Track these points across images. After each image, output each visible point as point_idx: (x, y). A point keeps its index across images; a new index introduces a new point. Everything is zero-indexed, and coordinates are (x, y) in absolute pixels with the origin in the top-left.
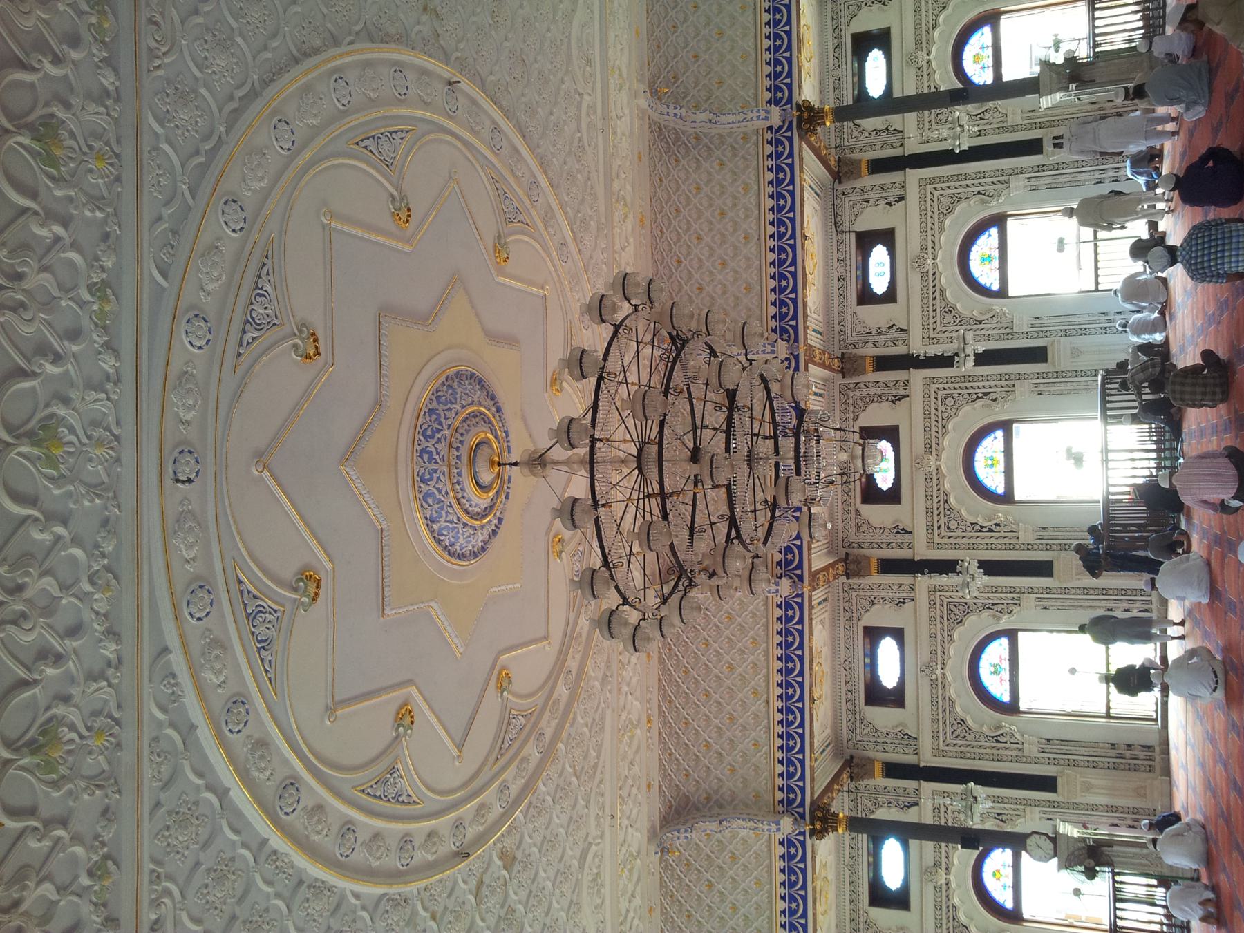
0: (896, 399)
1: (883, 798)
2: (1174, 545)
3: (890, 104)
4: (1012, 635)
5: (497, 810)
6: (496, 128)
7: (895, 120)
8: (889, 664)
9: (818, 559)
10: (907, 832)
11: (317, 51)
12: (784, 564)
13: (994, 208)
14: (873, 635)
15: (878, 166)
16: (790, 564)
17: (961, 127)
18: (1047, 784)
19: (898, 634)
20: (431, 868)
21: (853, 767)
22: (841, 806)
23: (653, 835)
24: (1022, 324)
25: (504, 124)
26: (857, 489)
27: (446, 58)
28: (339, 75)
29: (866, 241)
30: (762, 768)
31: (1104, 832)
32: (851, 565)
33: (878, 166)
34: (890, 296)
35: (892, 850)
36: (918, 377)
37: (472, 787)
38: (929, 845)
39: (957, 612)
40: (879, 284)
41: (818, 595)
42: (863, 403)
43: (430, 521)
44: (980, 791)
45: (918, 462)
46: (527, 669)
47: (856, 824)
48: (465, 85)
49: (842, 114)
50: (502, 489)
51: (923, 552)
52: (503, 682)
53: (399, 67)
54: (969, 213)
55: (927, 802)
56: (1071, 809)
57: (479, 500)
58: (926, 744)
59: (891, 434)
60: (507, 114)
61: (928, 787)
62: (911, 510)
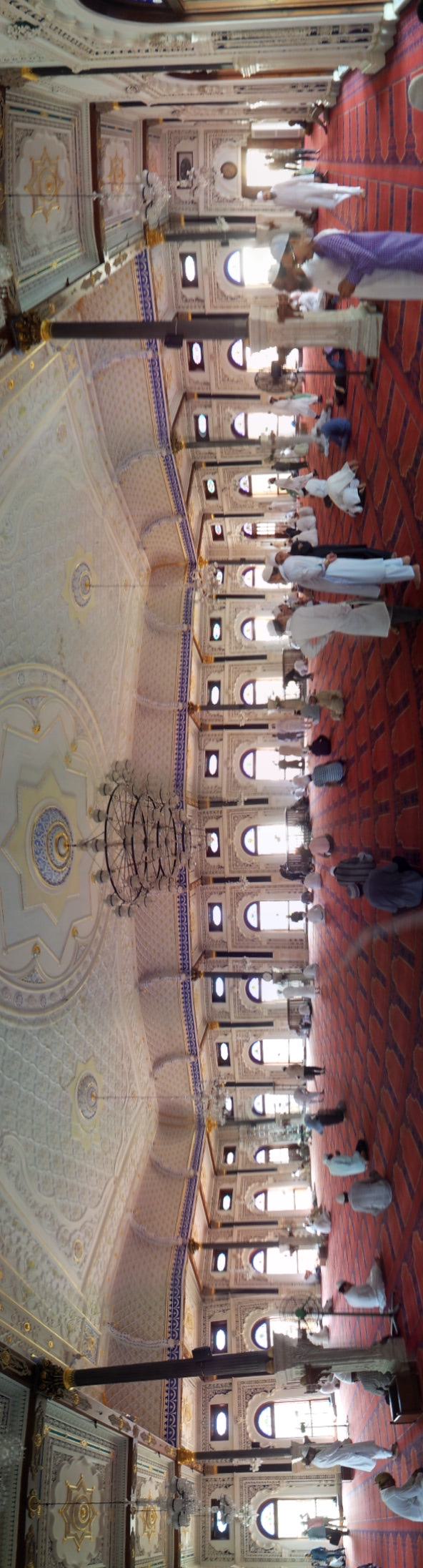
0: (218, 818)
1: (216, 965)
2: (309, 869)
3: (219, 707)
4: (258, 903)
5: (77, 982)
6: (79, 699)
7: (221, 712)
8: (217, 918)
9: (192, 878)
10: (224, 976)
11: (13, 663)
12: (179, 881)
13: (252, 746)
14: (211, 906)
15: (215, 727)
16: (182, 881)
17: (242, 717)
18: (269, 955)
19: (220, 905)
20: (53, 1006)
21: (206, 954)
22: (202, 968)
23: (136, 985)
24: (260, 789)
25: (83, 698)
26: (205, 852)
27: (64, 671)
28: (21, 673)
29: (209, 754)
30: (176, 960)
31: (287, 970)
32: (203, 880)
33: (215, 727)
34: (216, 775)
35: (219, 981)
36: (225, 809)
37: (66, 974)
38: (231, 980)
39: (239, 896)
40: (213, 771)
41: (192, 892)
42: (206, 819)
43: (41, 870)
44: (248, 959)
45: (226, 841)
46: (85, 926)
47: (207, 974)
48: (70, 682)
49: (203, 708)
50: (70, 857)
51: (228, 874)
52: (75, 933)
53: (45, 673)
54: (244, 748)
55: (230, 964)
56: (277, 963)
57: (60, 861)
58: (230, 943)
59: (216, 831)
60: (84, 694)
61: (231, 959)
62: (224, 860)
